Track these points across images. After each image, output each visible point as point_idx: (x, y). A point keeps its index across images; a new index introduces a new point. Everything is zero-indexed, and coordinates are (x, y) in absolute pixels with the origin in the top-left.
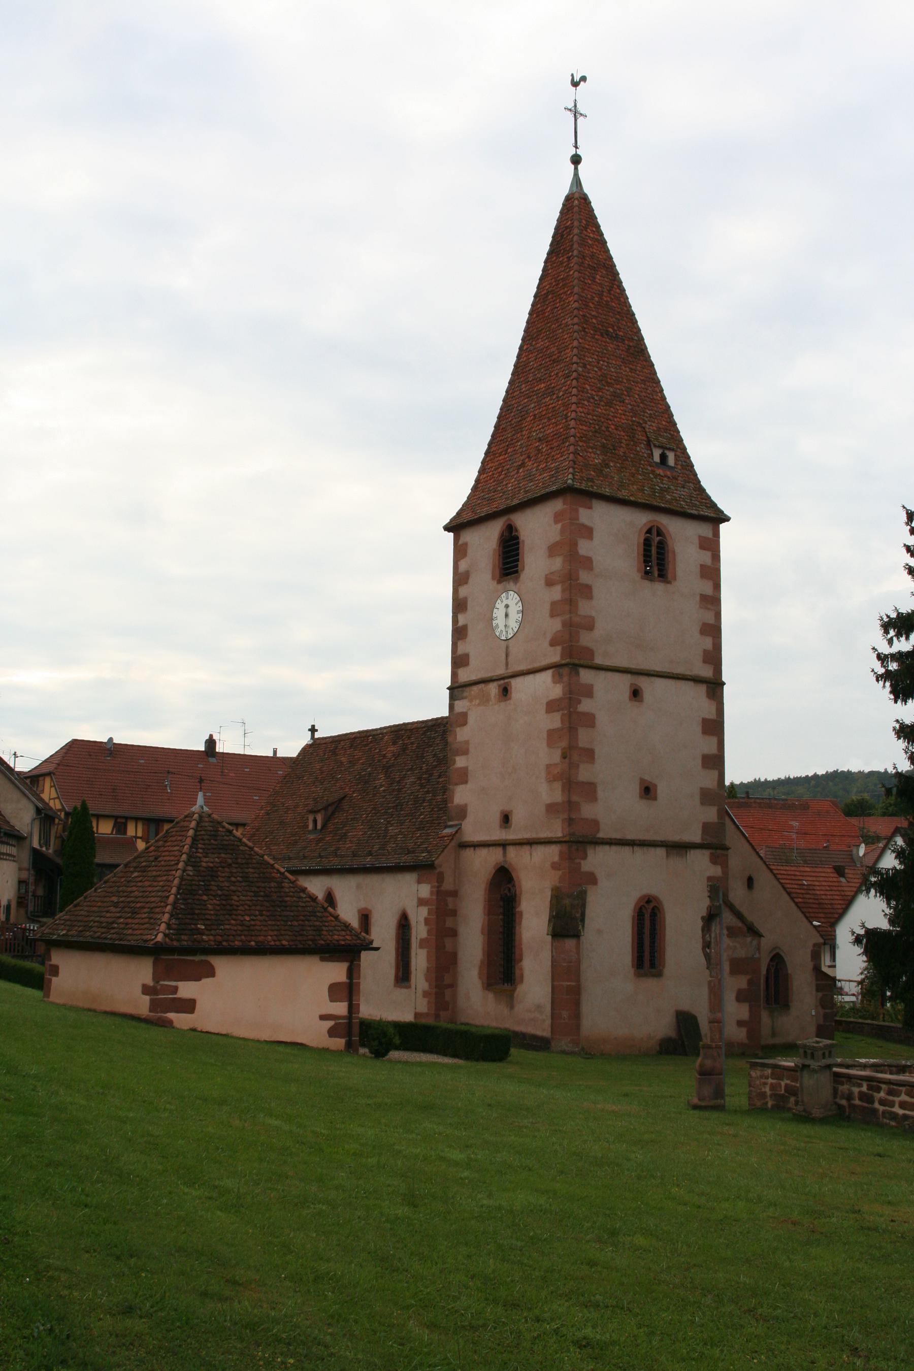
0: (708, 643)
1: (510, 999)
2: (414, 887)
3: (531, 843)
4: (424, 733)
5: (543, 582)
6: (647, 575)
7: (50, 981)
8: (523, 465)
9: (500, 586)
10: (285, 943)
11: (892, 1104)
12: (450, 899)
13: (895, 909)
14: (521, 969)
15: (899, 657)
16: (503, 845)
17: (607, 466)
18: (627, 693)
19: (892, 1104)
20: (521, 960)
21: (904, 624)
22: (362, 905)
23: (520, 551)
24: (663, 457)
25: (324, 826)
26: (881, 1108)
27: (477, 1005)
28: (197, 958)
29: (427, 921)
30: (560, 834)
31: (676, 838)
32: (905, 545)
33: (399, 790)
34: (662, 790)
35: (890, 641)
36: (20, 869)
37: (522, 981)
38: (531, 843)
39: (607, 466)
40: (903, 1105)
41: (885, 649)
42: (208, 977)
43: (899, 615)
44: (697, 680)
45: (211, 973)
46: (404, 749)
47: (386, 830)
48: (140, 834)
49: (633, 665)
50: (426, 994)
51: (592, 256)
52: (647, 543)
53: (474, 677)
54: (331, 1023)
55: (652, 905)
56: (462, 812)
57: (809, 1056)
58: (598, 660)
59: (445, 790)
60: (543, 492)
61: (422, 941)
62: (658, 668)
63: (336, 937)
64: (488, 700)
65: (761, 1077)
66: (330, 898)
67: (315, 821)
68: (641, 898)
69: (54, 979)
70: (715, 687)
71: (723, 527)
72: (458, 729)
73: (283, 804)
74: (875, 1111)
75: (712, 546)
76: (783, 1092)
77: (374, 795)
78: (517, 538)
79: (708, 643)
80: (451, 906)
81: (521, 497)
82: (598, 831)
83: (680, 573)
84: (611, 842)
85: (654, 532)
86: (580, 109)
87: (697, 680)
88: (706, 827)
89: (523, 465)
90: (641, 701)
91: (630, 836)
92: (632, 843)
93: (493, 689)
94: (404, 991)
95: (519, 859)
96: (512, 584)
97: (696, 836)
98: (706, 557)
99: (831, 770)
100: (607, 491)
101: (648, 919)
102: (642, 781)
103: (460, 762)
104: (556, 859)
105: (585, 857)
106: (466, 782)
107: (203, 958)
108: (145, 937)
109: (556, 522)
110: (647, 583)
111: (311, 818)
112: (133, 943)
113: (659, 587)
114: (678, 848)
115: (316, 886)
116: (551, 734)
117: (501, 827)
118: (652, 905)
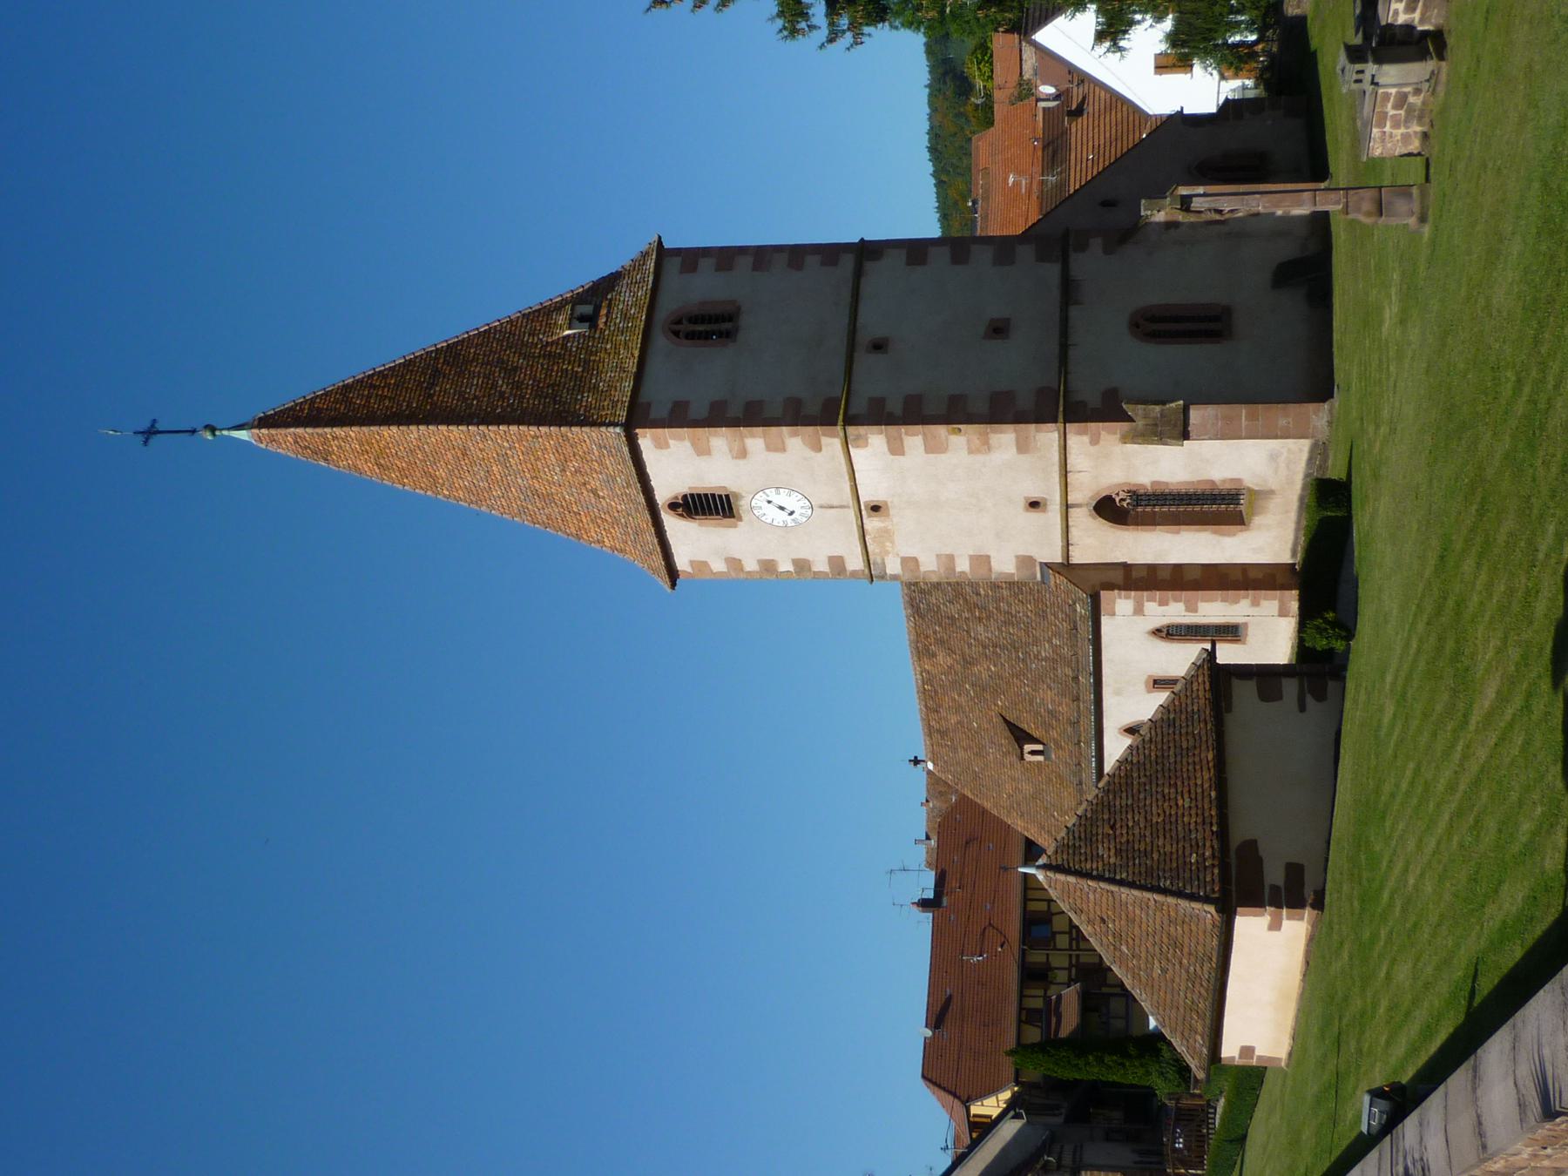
0: (812, 260)
1: (1260, 496)
2: (1118, 619)
4: (922, 617)
5: (741, 462)
6: (728, 335)
7: (1259, 1057)
8: (594, 492)
9: (745, 517)
10: (1210, 756)
13: (1145, 12)
14: (1224, 481)
16: (1067, 506)
20: (1213, 482)
21: (792, 10)
22: (1141, 687)
23: (702, 492)
25: (1037, 741)
27: (1272, 539)
29: (1163, 603)
30: (1056, 435)
31: (1056, 293)
33: (995, 646)
37: (1239, 480)
41: (824, 32)
42: (1257, 849)
43: (781, 14)
44: (858, 274)
45: (1251, 846)
46: (941, 642)
47: (1046, 659)
48: (1041, 992)
50: (1255, 603)
52: (691, 336)
53: (858, 549)
54: (1309, 699)
56: (1025, 561)
57: (1360, 76)
59: (995, 586)
60: (630, 463)
61: (1188, 609)
63: (1201, 694)
65: (1383, 141)
66: (1131, 730)
67: (1033, 753)
69: (1258, 1052)
70: (867, 251)
72: (922, 569)
73: (1010, 796)
75: (691, 258)
76: (1402, 112)
77: (1001, 677)
78: (685, 496)
79: (812, 260)
80: (1144, 573)
86: (145, 425)
87: (858, 274)
88: (1041, 258)
89: (594, 492)
91: (1054, 347)
92: (1064, 347)
93: (872, 524)
94: (1251, 631)
96: (742, 502)
97: (1052, 271)
98: (706, 264)
99: (927, 156)
100: (628, 385)
102: (987, 336)
103: (963, 566)
104: (1086, 439)
106: (988, 557)
107: (1233, 854)
108: (1209, 927)
109: (667, 446)
111: (1028, 758)
114: (1069, 291)
115: (1116, 747)
116: (929, 449)
117: (1044, 511)
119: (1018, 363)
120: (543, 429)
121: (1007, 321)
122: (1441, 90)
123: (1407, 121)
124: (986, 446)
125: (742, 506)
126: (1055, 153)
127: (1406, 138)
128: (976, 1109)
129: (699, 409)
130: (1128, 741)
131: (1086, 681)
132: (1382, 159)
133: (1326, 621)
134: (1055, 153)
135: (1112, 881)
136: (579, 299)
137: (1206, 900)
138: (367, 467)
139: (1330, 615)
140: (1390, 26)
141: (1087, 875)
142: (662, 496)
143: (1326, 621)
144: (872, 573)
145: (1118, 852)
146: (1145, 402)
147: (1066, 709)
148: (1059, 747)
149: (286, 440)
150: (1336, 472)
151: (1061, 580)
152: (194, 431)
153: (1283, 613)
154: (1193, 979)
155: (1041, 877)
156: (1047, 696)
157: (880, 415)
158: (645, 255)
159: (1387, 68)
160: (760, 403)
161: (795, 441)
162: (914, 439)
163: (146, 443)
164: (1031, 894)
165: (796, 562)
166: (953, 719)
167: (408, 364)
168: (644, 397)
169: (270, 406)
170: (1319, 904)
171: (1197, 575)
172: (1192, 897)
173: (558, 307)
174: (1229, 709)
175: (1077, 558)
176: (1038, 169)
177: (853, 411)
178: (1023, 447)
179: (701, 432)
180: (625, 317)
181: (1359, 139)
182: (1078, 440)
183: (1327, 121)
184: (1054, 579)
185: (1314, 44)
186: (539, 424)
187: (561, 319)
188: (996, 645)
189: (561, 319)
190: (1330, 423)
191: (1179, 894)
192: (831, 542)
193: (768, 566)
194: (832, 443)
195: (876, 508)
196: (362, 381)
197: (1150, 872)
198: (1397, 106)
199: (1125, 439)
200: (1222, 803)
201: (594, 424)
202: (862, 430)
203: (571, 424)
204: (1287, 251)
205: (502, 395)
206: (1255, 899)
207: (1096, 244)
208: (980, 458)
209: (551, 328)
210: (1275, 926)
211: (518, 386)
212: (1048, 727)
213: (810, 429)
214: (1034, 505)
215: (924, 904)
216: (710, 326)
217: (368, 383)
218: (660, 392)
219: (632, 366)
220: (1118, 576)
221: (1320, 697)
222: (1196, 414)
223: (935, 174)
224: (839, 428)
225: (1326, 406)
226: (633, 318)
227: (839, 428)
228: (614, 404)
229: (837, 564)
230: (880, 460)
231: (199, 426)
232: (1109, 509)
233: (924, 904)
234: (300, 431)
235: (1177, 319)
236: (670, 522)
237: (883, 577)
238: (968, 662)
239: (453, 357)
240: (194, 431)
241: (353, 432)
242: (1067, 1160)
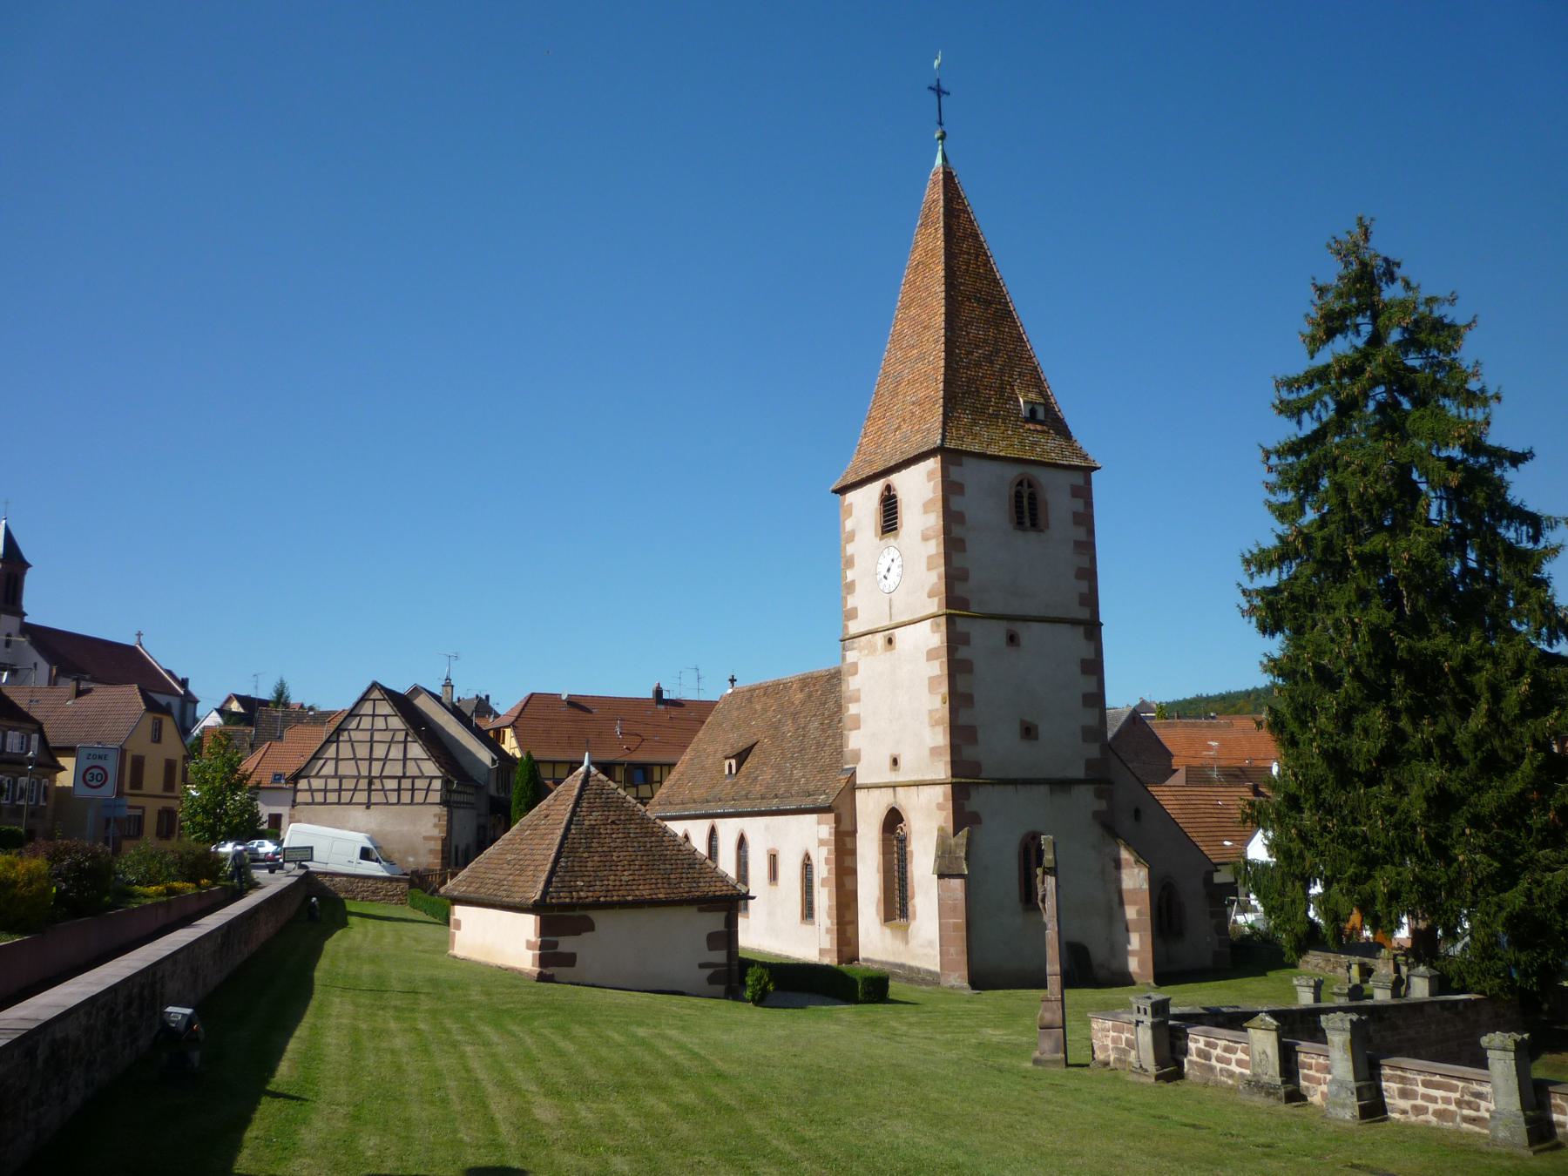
0: (1083, 586)
1: (904, 933)
6: (1019, 524)
8: (899, 428)
11: (1228, 1062)
12: (848, 839)
15: (1266, 592)
16: (894, 786)
19: (1228, 1062)
22: (771, 846)
26: (1219, 1066)
27: (876, 943)
28: (577, 913)
29: (827, 861)
31: (1060, 775)
32: (282, 684)
34: (1044, 729)
35: (1252, 576)
36: (479, 815)
40: (1240, 1063)
43: (1262, 551)
44: (1074, 622)
45: (590, 927)
49: (1009, 611)
52: (1018, 496)
53: (863, 629)
54: (708, 972)
56: (857, 756)
62: (1034, 612)
64: (875, 651)
66: (687, 837)
68: (1027, 835)
70: (1092, 628)
71: (1094, 475)
74: (1211, 1069)
75: (1084, 493)
79: (1083, 586)
80: (849, 846)
81: (898, 458)
86: (944, 86)
87: (1074, 622)
88: (1090, 764)
89: (899, 428)
91: (1012, 776)
92: (1014, 782)
93: (880, 639)
94: (810, 927)
97: (1079, 772)
98: (1079, 505)
100: (976, 448)
102: (1023, 722)
103: (853, 709)
104: (941, 800)
105: (968, 798)
107: (583, 913)
110: (1020, 533)
114: (1061, 785)
115: (677, 828)
116: (932, 680)
119: (999, 746)
120: (941, 386)
121: (1036, 738)
122: (1132, 1078)
123: (1116, 1049)
124: (935, 724)
125: (890, 540)
126: (1236, 776)
127: (1105, 1048)
128: (509, 732)
129: (957, 504)
130: (680, 834)
131: (774, 804)
132: (1090, 1028)
133: (766, 984)
134: (1236, 776)
135: (570, 822)
136: (1049, 408)
137: (545, 893)
138: (917, 256)
139: (771, 987)
140: (1187, 1036)
141: (577, 804)
142: (896, 479)
143: (766, 984)
144: (847, 640)
145: (592, 827)
146: (968, 845)
147: (758, 789)
148: (734, 785)
149: (934, 194)
150: (894, 988)
151: (843, 782)
152: (940, 124)
153: (822, 952)
154: (499, 883)
155: (582, 769)
156: (767, 776)
157: (955, 641)
158: (1085, 457)
159: (1149, 1033)
160: (964, 550)
161: (934, 577)
162: (938, 668)
163: (930, 88)
164: (665, 769)
165: (853, 582)
166: (758, 707)
167: (996, 282)
168: (966, 460)
169: (961, 179)
170: (542, 978)
171: (848, 886)
172: (548, 883)
173: (1043, 393)
174: (700, 910)
175: (860, 795)
176: (1223, 763)
177: (958, 620)
178: (934, 751)
179: (940, 504)
180: (1034, 444)
181: (1106, 1010)
182: (940, 794)
183: (1204, 984)
184: (844, 777)
185: (1271, 974)
186: (946, 382)
187: (1032, 396)
188: (793, 740)
189: (1032, 396)
190: (952, 987)
191: (552, 872)
192: (867, 609)
193: (850, 563)
194: (935, 605)
195: (890, 641)
196: (981, 246)
197: (573, 850)
198: (1128, 1041)
199: (941, 830)
200: (623, 905)
201: (945, 424)
202: (944, 628)
203: (945, 406)
204: (1098, 953)
205: (970, 353)
206: (547, 929)
207: (1102, 805)
208: (926, 720)
209: (1026, 388)
210: (529, 946)
211: (978, 365)
212: (747, 777)
213: (943, 588)
214: (895, 762)
215: (659, 692)
216: (1027, 509)
217: (980, 252)
218: (969, 472)
219: (993, 450)
220: (846, 826)
221: (712, 980)
222: (958, 884)
223: (1256, 690)
224: (944, 611)
225: (966, 984)
226: (1033, 450)
227: (944, 611)
228: (961, 439)
229: (852, 614)
230: (925, 641)
231: (945, 128)
232: (893, 820)
233: (659, 692)
234: (941, 203)
236: (877, 487)
237: (844, 649)
238: (795, 716)
239: (1000, 314)
240: (940, 124)
241: (941, 244)
242: (455, 797)
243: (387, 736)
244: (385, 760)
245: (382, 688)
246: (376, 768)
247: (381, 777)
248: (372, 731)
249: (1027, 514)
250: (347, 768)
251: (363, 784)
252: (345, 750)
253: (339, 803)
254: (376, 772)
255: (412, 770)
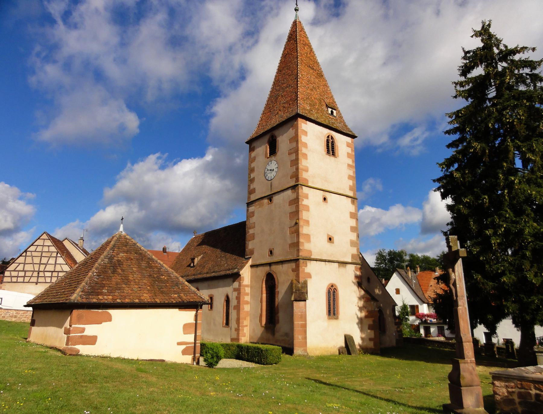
3: (282, 262)
6: (328, 152)
8: (278, 113)
16: (270, 264)
17: (312, 111)
18: (322, 199)
20: (278, 313)
24: (332, 112)
34: (336, 239)
37: (278, 322)
38: (282, 262)
39: (312, 111)
45: (109, 319)
49: (324, 188)
51: (303, 41)
52: (328, 141)
54: (184, 347)
55: (334, 288)
58: (310, 184)
82: (311, 255)
83: (340, 154)
84: (316, 260)
85: (330, 137)
88: (353, 256)
90: (327, 202)
91: (324, 258)
92: (325, 261)
95: (277, 270)
101: (332, 294)
102: (328, 235)
105: (306, 266)
112: (61, 302)
113: (332, 158)
118: (334, 288)
147: (205, 271)
160: (307, 159)
214: (271, 252)
235: (334, 299)
243: (48, 254)
244: (46, 264)
245: (48, 235)
246: (42, 268)
247: (44, 271)
248: (42, 252)
249: (330, 149)
250: (28, 267)
251: (36, 274)
252: (29, 260)
253: (24, 282)
254: (42, 269)
255: (58, 268)
